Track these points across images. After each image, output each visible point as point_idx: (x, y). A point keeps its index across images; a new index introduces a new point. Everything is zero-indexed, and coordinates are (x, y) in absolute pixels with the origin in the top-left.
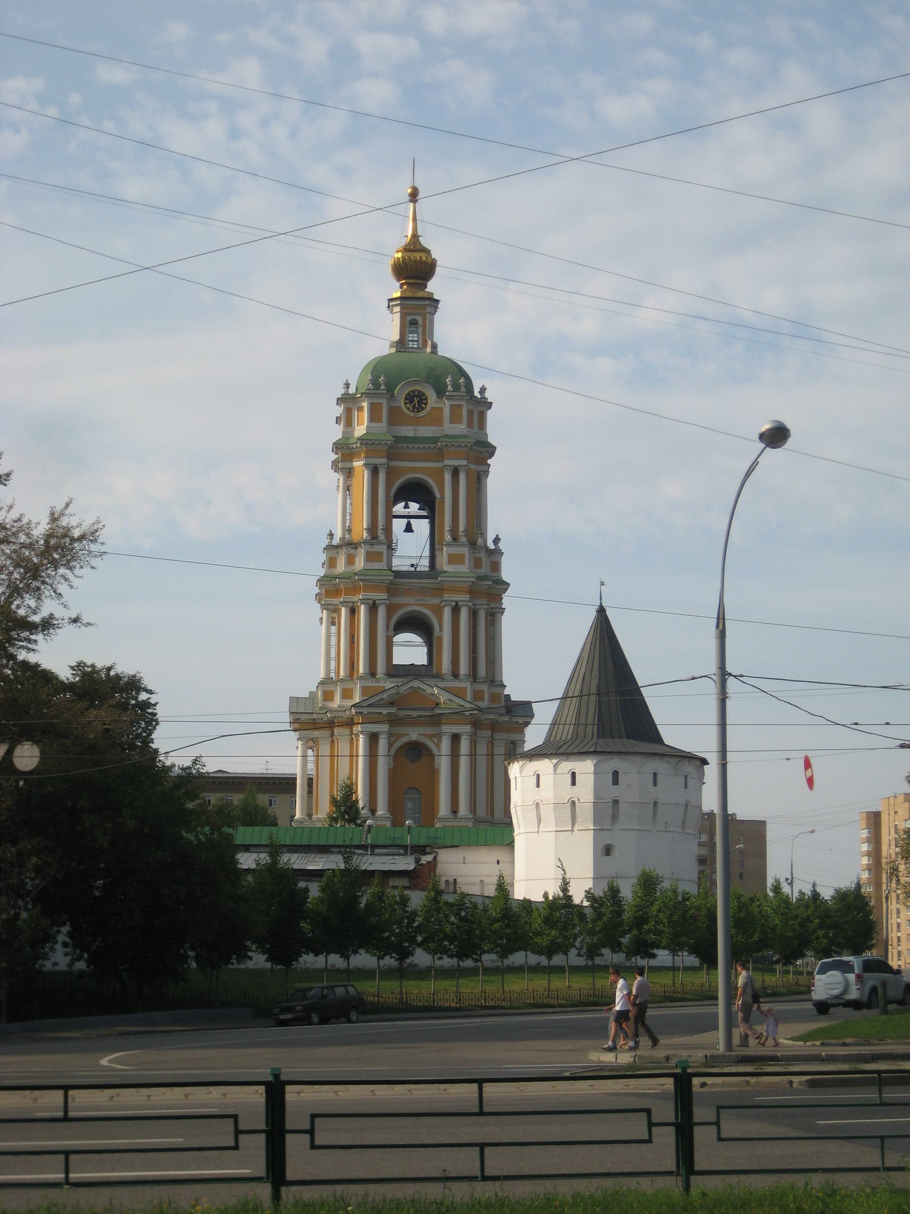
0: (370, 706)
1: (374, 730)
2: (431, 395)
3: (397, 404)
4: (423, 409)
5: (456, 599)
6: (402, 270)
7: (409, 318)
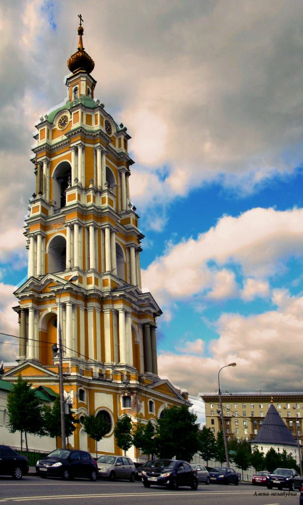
0: (23, 292)
1: (25, 307)
2: (68, 115)
3: (55, 128)
4: (66, 124)
5: (70, 221)
6: (73, 66)
7: (74, 88)
